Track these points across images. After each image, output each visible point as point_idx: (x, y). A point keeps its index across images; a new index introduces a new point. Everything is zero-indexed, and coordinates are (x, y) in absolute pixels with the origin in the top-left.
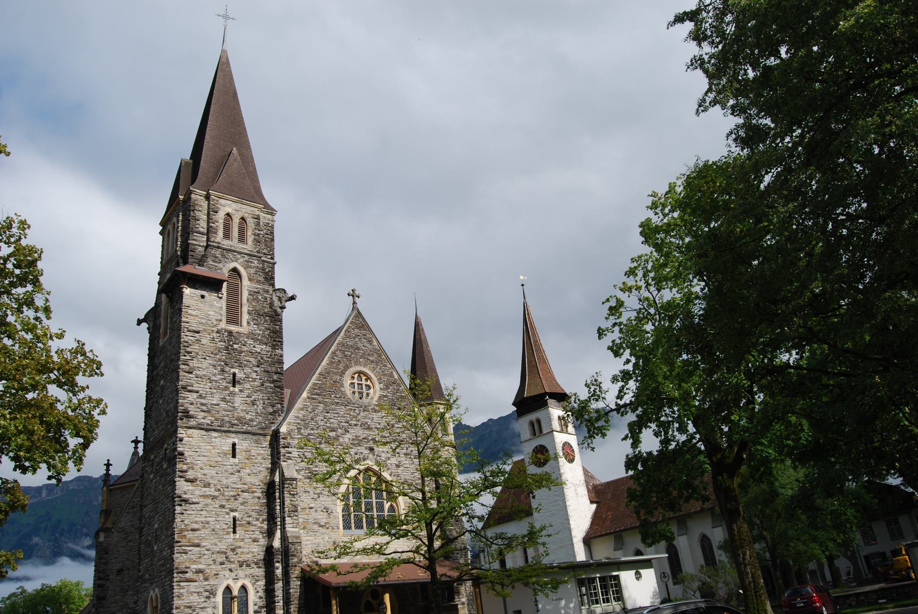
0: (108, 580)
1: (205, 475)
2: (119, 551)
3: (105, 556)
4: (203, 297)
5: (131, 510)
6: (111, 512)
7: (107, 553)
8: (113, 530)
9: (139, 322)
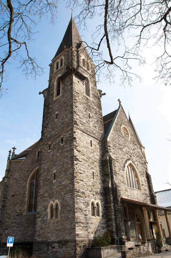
0: (7, 199)
1: (83, 150)
2: (13, 187)
3: (7, 188)
4: (79, 82)
5: (20, 171)
6: (10, 171)
7: (8, 187)
8: (11, 178)
9: (40, 93)
